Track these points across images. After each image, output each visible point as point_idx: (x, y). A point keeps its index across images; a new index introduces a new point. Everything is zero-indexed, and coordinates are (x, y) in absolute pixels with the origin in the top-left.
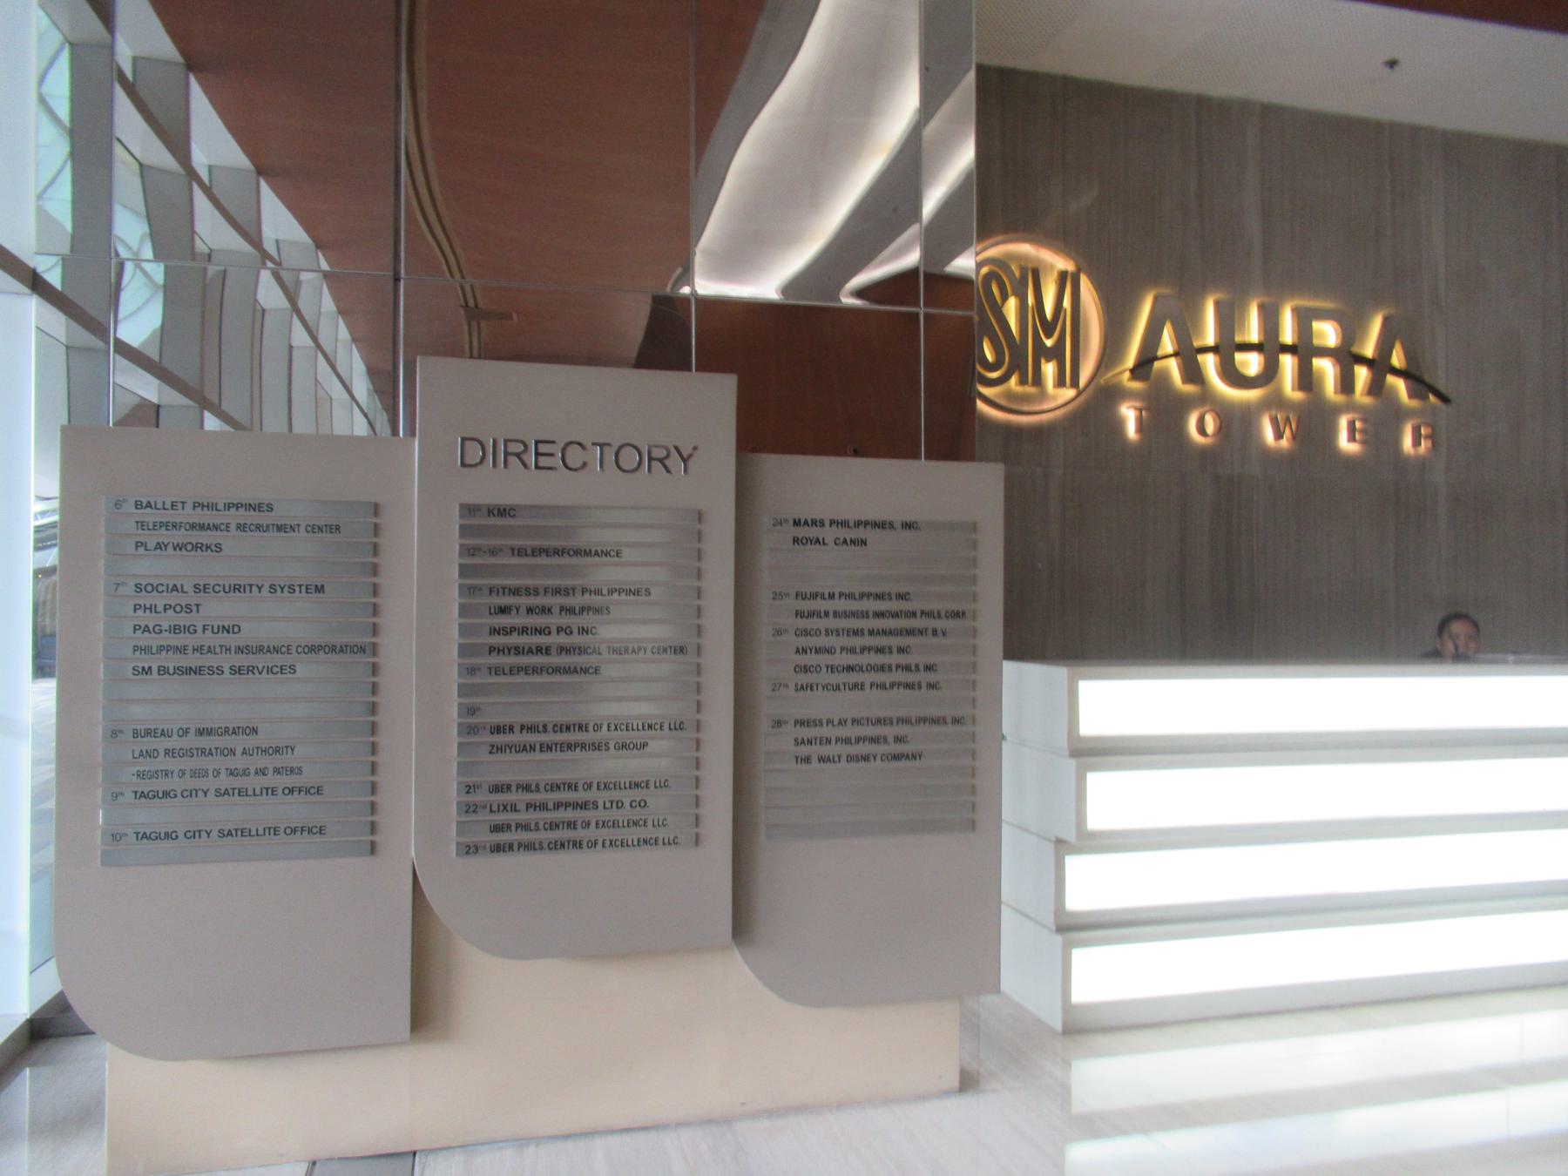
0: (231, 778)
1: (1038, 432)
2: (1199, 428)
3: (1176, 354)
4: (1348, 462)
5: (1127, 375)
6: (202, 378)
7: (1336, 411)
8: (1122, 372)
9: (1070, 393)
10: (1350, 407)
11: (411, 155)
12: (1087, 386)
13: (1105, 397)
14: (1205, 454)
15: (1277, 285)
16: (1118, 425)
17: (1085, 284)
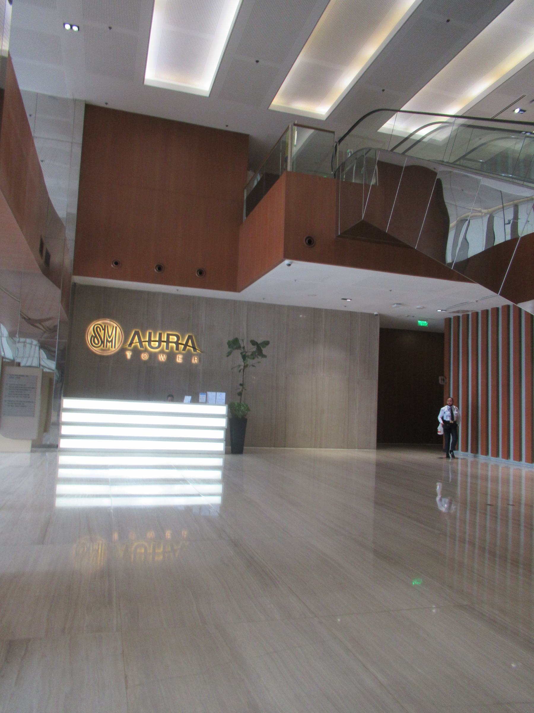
0: (446, 416)
1: (108, 357)
2: (145, 357)
3: (139, 342)
4: (179, 364)
5: (128, 346)
6: (505, 226)
7: (176, 354)
8: (127, 345)
9: (115, 349)
10: (180, 353)
11: (405, 143)
12: (117, 348)
13: (123, 351)
14: (145, 362)
15: (164, 328)
16: (125, 356)
17: (118, 328)
